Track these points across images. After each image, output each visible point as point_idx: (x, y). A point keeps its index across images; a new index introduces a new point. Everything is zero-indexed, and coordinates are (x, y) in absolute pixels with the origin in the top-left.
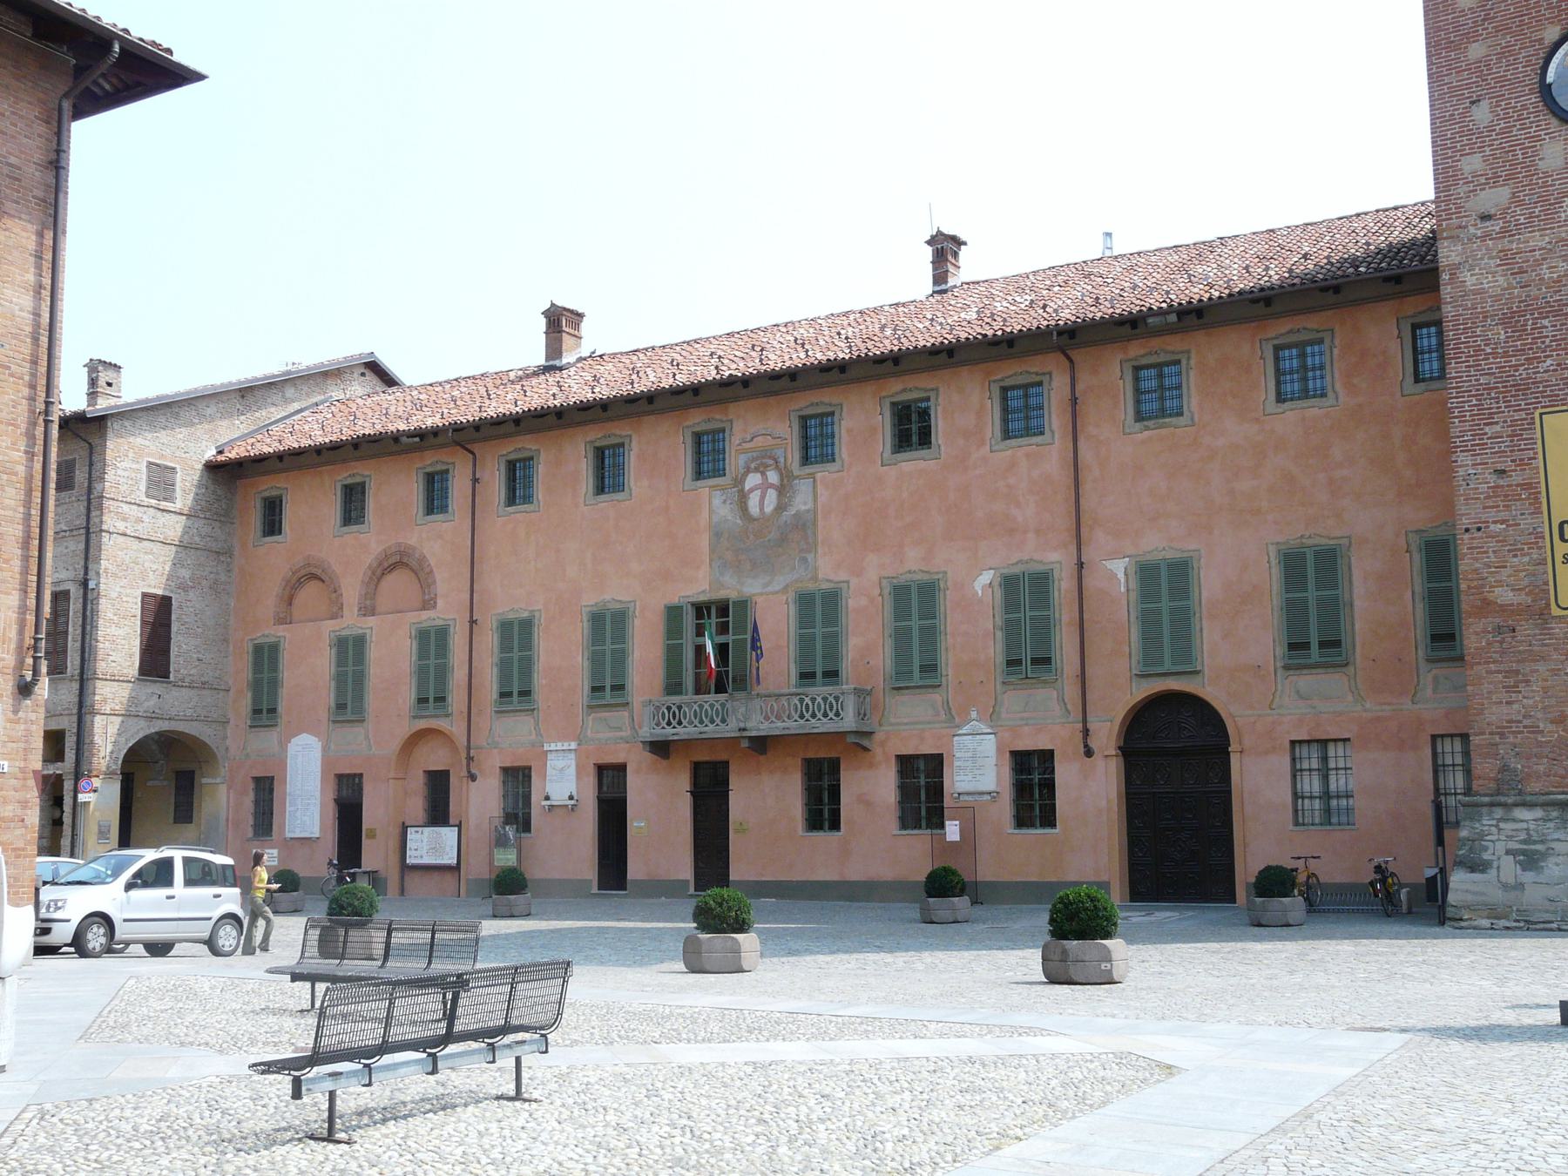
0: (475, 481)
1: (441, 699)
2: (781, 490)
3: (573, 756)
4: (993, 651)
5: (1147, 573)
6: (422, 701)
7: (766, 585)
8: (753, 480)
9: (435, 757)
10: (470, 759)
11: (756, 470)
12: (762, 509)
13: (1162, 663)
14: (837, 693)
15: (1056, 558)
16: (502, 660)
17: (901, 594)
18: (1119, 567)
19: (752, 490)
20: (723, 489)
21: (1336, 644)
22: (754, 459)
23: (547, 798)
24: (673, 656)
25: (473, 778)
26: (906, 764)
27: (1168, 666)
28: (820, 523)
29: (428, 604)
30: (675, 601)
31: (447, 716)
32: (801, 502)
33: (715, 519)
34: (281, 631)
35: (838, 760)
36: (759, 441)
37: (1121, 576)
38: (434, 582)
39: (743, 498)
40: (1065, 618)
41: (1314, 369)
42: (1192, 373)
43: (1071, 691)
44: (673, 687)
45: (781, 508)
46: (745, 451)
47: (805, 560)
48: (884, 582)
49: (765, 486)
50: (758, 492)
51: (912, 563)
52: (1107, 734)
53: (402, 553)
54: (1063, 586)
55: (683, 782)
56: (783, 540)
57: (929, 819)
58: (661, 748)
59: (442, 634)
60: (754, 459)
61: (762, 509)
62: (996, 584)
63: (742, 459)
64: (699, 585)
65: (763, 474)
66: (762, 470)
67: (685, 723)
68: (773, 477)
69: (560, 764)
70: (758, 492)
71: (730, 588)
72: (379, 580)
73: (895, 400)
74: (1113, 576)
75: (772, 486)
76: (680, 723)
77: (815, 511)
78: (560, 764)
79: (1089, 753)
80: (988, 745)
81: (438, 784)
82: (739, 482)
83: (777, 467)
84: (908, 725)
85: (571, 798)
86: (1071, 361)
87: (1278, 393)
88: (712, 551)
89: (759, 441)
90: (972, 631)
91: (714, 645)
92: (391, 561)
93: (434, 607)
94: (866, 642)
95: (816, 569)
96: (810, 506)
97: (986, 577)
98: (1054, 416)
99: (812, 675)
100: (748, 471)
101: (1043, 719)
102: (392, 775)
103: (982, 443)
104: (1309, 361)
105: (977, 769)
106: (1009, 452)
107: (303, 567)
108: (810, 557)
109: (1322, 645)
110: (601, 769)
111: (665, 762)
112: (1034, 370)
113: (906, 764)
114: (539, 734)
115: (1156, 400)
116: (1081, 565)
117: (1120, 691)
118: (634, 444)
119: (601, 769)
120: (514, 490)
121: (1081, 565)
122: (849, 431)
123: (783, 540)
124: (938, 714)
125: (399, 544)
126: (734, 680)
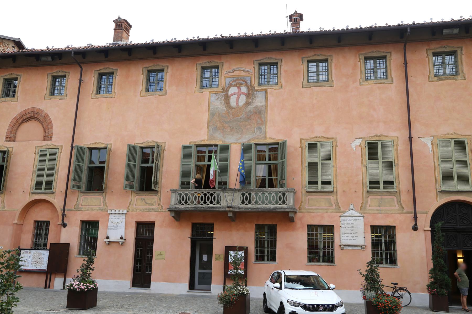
0: (81, 81)
1: (49, 185)
2: (248, 95)
3: (124, 216)
4: (363, 176)
5: (444, 146)
6: (38, 185)
7: (238, 139)
8: (233, 90)
9: (41, 214)
10: (64, 216)
11: (235, 86)
12: (237, 103)
13: (453, 187)
14: (283, 191)
15: (397, 135)
16: (310, 165)
17: (312, 148)
18: (428, 141)
19: (232, 95)
20: (217, 93)
21: (329, 183)
22: (236, 80)
23: (108, 238)
24: (185, 170)
25: (64, 225)
26: (313, 230)
27: (456, 188)
28: (269, 111)
29: (47, 137)
30: (187, 144)
31: (53, 193)
32: (259, 101)
33: (212, 107)
34: (10, 145)
35: (276, 225)
36: (237, 73)
37: (429, 145)
38: (52, 128)
39: (227, 98)
40: (400, 163)
41: (215, 78)
42: (463, 57)
43: (406, 198)
44: (184, 184)
45: (247, 104)
46: (229, 77)
47: (260, 128)
48: (303, 141)
49: (239, 94)
50: (236, 96)
51: (318, 132)
52: (425, 222)
53: (34, 113)
54: (400, 148)
55: (187, 233)
56: (249, 118)
57: (387, 260)
58: (178, 215)
59: (269, 149)
60: (236, 80)
61: (237, 103)
62: (363, 145)
63: (228, 80)
64: (201, 136)
65: (239, 88)
66: (238, 86)
67: (189, 202)
68: (244, 89)
69: (116, 221)
70: (236, 96)
71: (219, 140)
72: (20, 124)
73: (100, 72)
74: (425, 145)
75: (243, 93)
76: (186, 202)
77: (266, 106)
78: (116, 221)
79: (415, 228)
80: (122, 220)
81: (42, 227)
82: (225, 90)
83: (246, 85)
84: (316, 211)
85: (122, 238)
86: (81, 67)
87: (259, 83)
88: (209, 121)
89: (237, 73)
90: (350, 166)
91: (202, 167)
92: (28, 116)
93: (51, 139)
94: (297, 171)
95: (266, 133)
96: (264, 103)
97: (358, 142)
98: (393, 72)
99: (41, 185)
100: (230, 85)
101: (390, 213)
102: (16, 222)
103: (354, 81)
104: (321, 68)
105: (353, 233)
106: (369, 86)
107: (31, 113)
108: (263, 127)
109: (323, 183)
110: (139, 224)
111: (177, 223)
112: (382, 51)
113: (313, 230)
114: (105, 204)
115: (153, 83)
116: (410, 138)
117: (431, 202)
118: (169, 70)
119: (139, 224)
120: (54, 90)
121: (410, 138)
122: (286, 71)
123: (249, 118)
124: (332, 205)
125: (34, 108)
126: (219, 183)
